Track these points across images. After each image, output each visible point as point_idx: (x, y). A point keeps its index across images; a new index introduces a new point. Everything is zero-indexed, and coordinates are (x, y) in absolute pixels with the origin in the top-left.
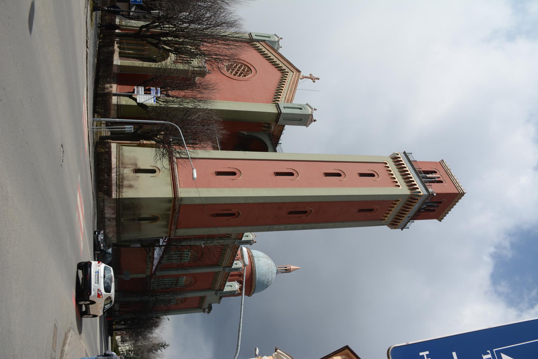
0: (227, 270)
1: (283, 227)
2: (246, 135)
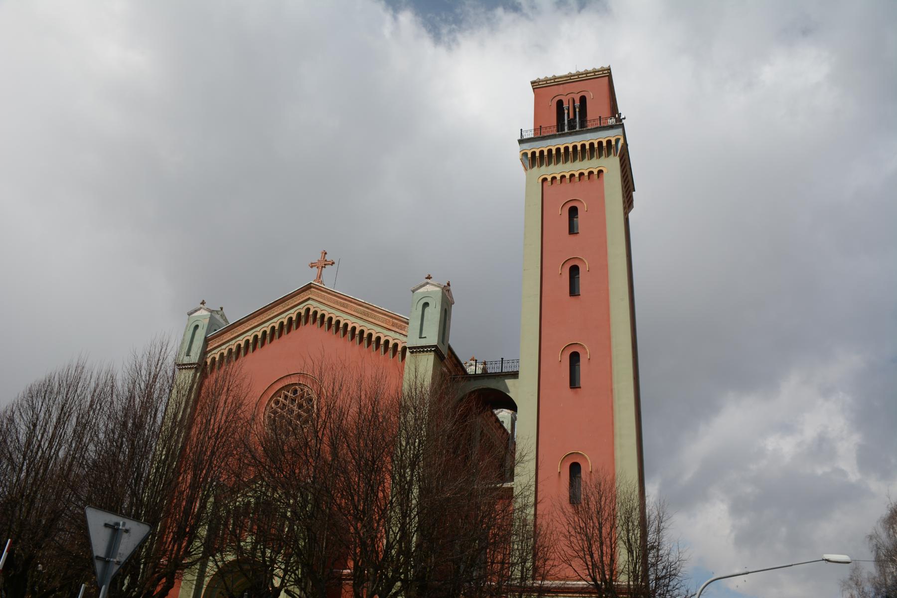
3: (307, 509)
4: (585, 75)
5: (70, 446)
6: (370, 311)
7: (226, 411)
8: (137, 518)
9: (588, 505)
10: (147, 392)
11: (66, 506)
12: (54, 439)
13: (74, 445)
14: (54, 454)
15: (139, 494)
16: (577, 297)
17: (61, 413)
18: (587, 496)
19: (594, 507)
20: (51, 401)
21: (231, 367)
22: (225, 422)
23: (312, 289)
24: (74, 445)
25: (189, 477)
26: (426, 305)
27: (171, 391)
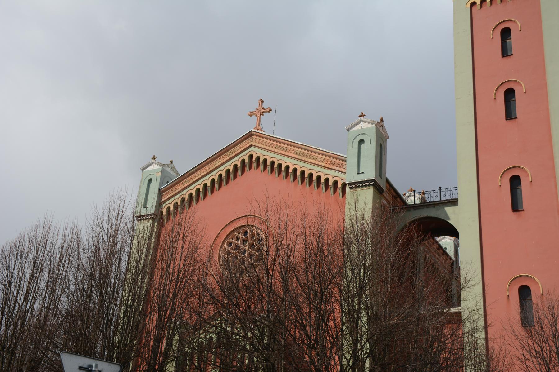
3: (264, 341)
5: (44, 299)
6: (309, 153)
7: (184, 256)
8: (109, 359)
9: (542, 328)
10: (110, 244)
11: (44, 354)
12: (29, 294)
13: (47, 298)
14: (30, 307)
15: (110, 337)
16: (514, 120)
17: (33, 269)
18: (540, 319)
19: (548, 330)
20: (23, 260)
21: (185, 215)
22: (184, 266)
23: (253, 136)
24: (47, 298)
25: (155, 318)
26: (362, 141)
27: (132, 241)
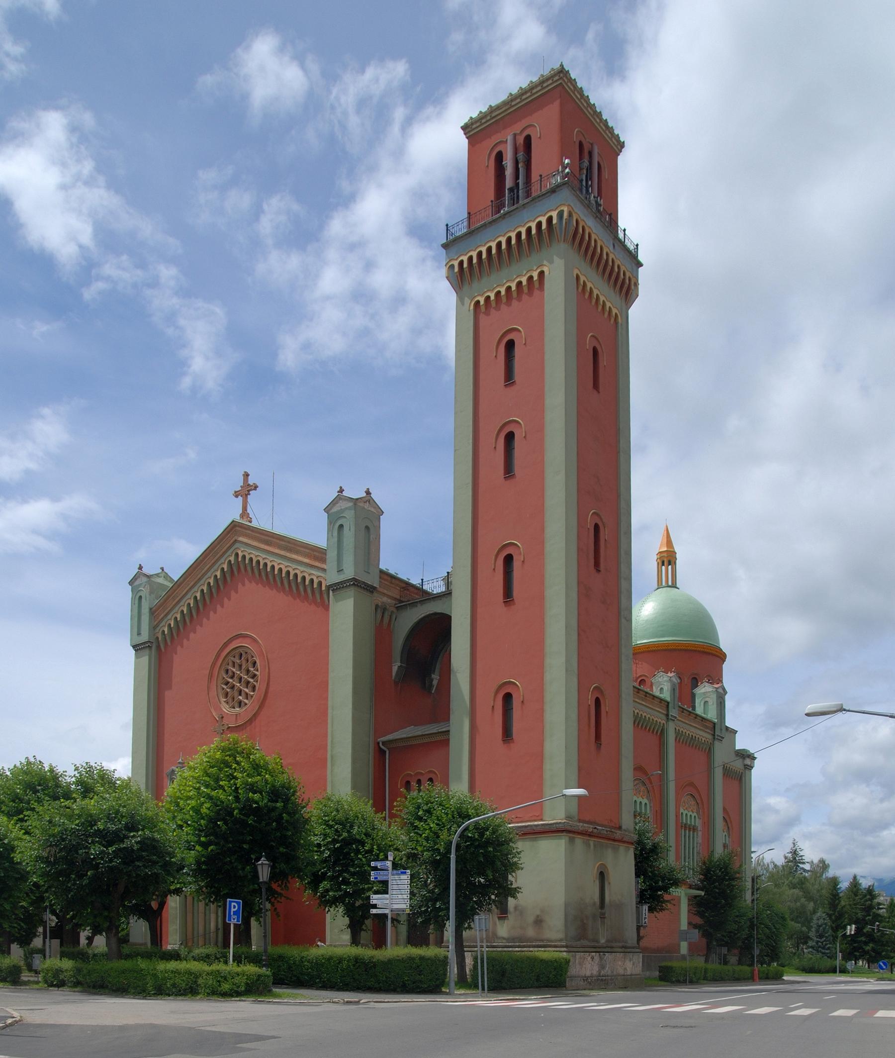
0: (673, 712)
1: (624, 584)
2: (401, 666)
4: (539, 88)
